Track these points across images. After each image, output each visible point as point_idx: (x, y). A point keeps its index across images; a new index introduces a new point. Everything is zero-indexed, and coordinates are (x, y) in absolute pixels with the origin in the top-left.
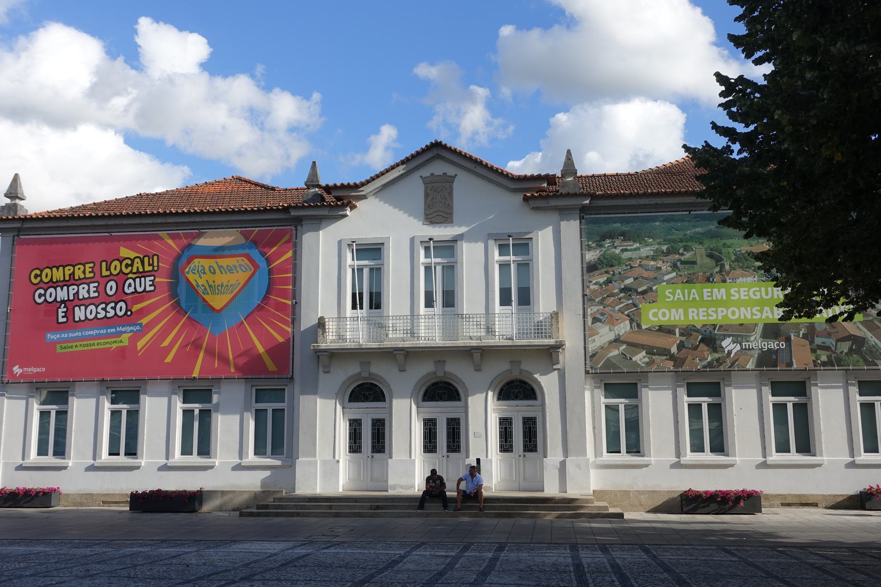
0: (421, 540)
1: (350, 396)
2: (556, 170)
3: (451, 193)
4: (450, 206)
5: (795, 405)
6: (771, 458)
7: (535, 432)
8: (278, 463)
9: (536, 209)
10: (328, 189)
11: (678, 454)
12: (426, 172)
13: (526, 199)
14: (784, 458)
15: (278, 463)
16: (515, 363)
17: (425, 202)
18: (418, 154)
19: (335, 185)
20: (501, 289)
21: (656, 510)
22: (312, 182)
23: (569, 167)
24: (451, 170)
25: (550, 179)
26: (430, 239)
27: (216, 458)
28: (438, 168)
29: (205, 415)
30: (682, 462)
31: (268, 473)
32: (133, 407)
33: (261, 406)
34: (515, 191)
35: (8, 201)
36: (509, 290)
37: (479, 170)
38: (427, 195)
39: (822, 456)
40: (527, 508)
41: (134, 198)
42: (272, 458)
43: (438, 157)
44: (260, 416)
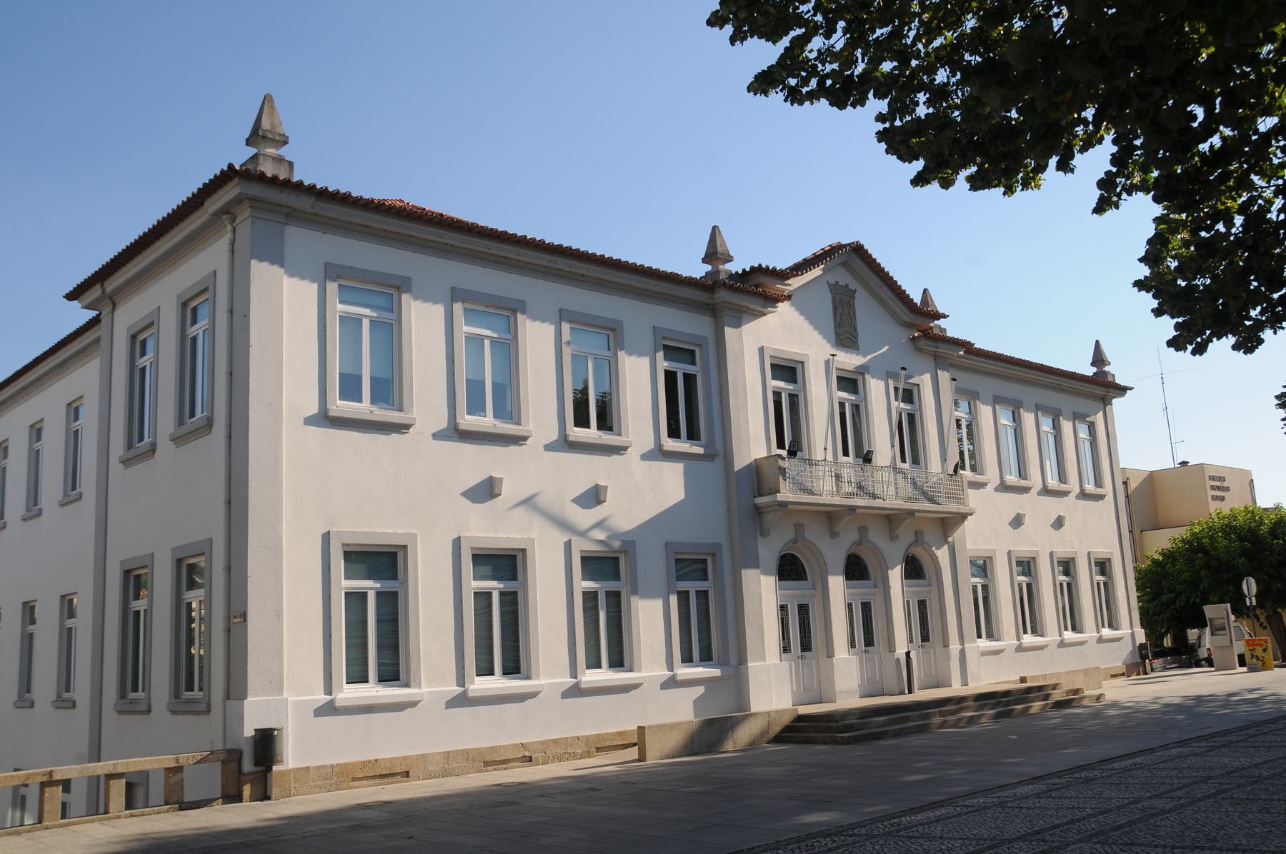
5: (379, 595)
6: (472, 687)
8: (715, 672)
11: (461, 681)
14: (380, 693)
15: (715, 672)
19: (744, 270)
20: (494, 384)
21: (669, 757)
27: (419, 686)
29: (615, 600)
30: (471, 695)
31: (700, 690)
32: (389, 585)
33: (683, 586)
35: (708, 268)
36: (482, 384)
39: (419, 686)
40: (907, 719)
42: (704, 666)
44: (683, 596)
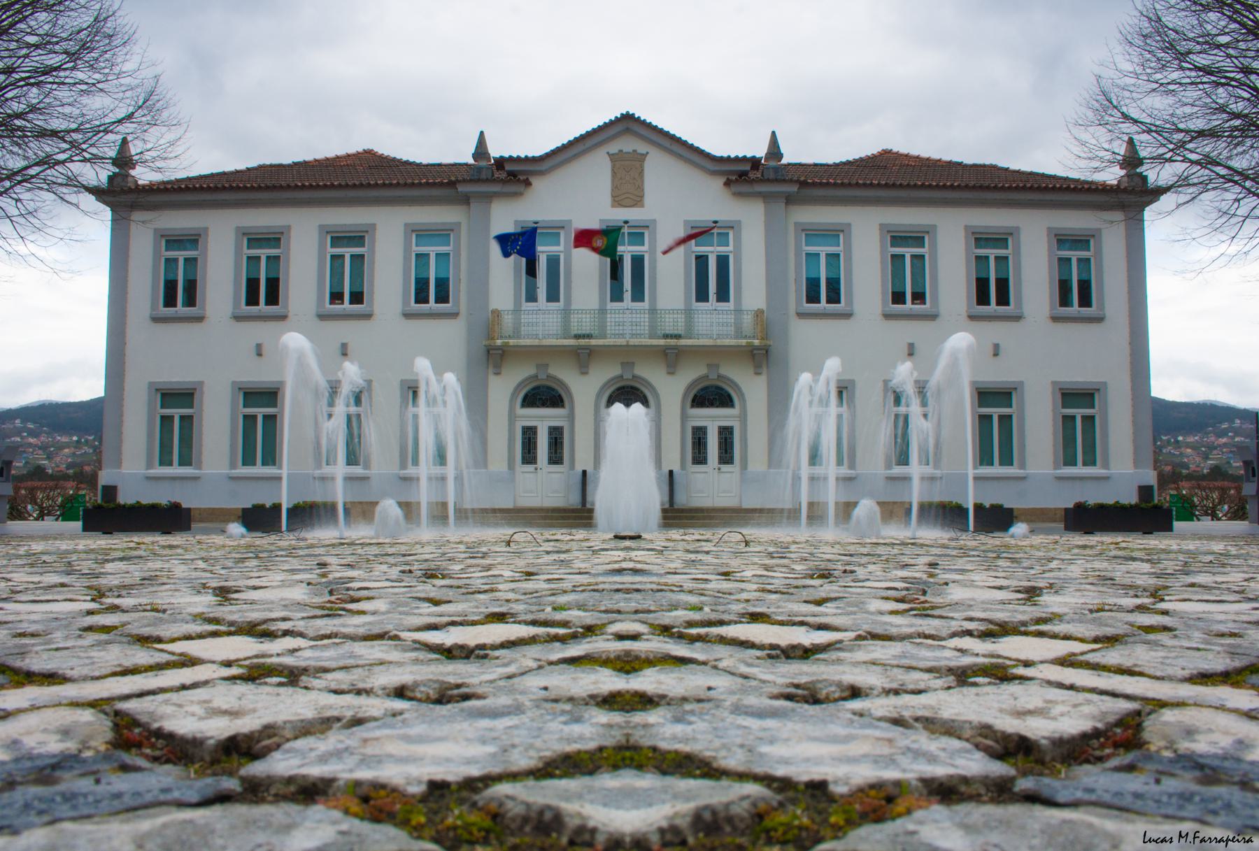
0: (1001, 616)
1: (693, 401)
2: (760, 151)
3: (641, 173)
4: (641, 188)
7: (732, 443)
9: (739, 195)
10: (501, 162)
12: (614, 147)
13: (728, 184)
16: (628, 365)
17: (613, 181)
18: (612, 123)
22: (481, 150)
23: (774, 151)
24: (641, 147)
25: (755, 162)
26: (626, 222)
28: (628, 145)
34: (714, 173)
37: (676, 148)
38: (614, 173)
41: (232, 173)
43: (628, 131)
